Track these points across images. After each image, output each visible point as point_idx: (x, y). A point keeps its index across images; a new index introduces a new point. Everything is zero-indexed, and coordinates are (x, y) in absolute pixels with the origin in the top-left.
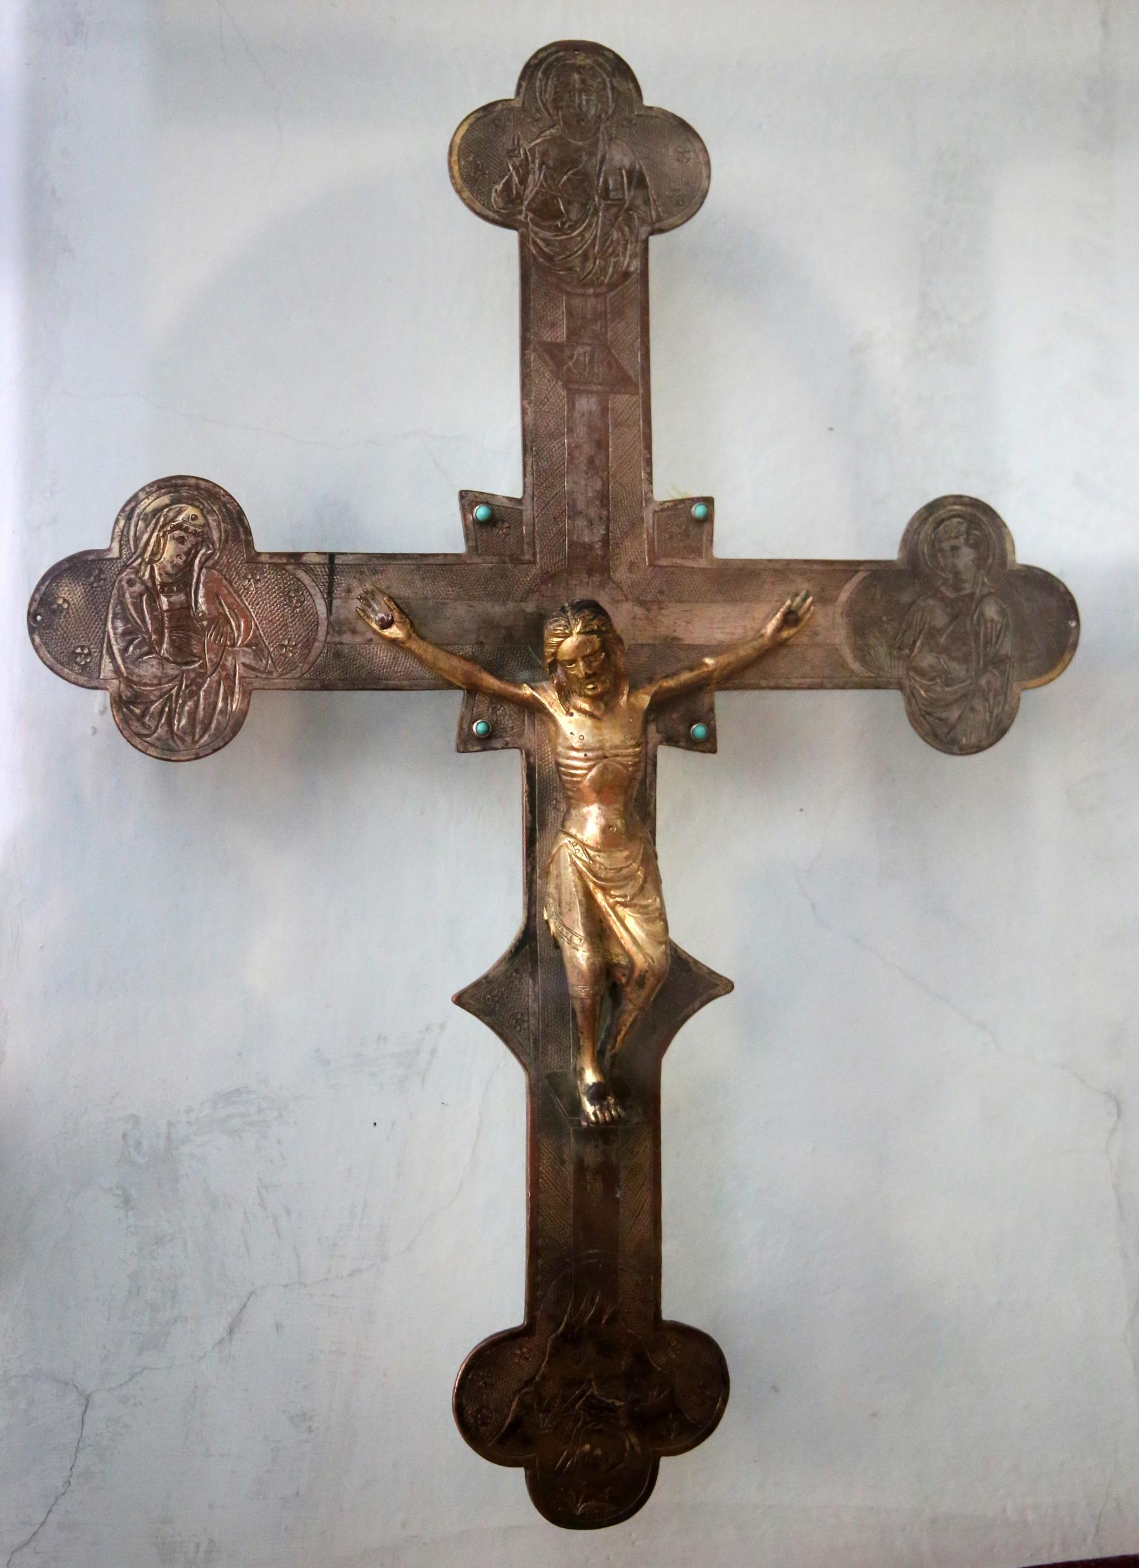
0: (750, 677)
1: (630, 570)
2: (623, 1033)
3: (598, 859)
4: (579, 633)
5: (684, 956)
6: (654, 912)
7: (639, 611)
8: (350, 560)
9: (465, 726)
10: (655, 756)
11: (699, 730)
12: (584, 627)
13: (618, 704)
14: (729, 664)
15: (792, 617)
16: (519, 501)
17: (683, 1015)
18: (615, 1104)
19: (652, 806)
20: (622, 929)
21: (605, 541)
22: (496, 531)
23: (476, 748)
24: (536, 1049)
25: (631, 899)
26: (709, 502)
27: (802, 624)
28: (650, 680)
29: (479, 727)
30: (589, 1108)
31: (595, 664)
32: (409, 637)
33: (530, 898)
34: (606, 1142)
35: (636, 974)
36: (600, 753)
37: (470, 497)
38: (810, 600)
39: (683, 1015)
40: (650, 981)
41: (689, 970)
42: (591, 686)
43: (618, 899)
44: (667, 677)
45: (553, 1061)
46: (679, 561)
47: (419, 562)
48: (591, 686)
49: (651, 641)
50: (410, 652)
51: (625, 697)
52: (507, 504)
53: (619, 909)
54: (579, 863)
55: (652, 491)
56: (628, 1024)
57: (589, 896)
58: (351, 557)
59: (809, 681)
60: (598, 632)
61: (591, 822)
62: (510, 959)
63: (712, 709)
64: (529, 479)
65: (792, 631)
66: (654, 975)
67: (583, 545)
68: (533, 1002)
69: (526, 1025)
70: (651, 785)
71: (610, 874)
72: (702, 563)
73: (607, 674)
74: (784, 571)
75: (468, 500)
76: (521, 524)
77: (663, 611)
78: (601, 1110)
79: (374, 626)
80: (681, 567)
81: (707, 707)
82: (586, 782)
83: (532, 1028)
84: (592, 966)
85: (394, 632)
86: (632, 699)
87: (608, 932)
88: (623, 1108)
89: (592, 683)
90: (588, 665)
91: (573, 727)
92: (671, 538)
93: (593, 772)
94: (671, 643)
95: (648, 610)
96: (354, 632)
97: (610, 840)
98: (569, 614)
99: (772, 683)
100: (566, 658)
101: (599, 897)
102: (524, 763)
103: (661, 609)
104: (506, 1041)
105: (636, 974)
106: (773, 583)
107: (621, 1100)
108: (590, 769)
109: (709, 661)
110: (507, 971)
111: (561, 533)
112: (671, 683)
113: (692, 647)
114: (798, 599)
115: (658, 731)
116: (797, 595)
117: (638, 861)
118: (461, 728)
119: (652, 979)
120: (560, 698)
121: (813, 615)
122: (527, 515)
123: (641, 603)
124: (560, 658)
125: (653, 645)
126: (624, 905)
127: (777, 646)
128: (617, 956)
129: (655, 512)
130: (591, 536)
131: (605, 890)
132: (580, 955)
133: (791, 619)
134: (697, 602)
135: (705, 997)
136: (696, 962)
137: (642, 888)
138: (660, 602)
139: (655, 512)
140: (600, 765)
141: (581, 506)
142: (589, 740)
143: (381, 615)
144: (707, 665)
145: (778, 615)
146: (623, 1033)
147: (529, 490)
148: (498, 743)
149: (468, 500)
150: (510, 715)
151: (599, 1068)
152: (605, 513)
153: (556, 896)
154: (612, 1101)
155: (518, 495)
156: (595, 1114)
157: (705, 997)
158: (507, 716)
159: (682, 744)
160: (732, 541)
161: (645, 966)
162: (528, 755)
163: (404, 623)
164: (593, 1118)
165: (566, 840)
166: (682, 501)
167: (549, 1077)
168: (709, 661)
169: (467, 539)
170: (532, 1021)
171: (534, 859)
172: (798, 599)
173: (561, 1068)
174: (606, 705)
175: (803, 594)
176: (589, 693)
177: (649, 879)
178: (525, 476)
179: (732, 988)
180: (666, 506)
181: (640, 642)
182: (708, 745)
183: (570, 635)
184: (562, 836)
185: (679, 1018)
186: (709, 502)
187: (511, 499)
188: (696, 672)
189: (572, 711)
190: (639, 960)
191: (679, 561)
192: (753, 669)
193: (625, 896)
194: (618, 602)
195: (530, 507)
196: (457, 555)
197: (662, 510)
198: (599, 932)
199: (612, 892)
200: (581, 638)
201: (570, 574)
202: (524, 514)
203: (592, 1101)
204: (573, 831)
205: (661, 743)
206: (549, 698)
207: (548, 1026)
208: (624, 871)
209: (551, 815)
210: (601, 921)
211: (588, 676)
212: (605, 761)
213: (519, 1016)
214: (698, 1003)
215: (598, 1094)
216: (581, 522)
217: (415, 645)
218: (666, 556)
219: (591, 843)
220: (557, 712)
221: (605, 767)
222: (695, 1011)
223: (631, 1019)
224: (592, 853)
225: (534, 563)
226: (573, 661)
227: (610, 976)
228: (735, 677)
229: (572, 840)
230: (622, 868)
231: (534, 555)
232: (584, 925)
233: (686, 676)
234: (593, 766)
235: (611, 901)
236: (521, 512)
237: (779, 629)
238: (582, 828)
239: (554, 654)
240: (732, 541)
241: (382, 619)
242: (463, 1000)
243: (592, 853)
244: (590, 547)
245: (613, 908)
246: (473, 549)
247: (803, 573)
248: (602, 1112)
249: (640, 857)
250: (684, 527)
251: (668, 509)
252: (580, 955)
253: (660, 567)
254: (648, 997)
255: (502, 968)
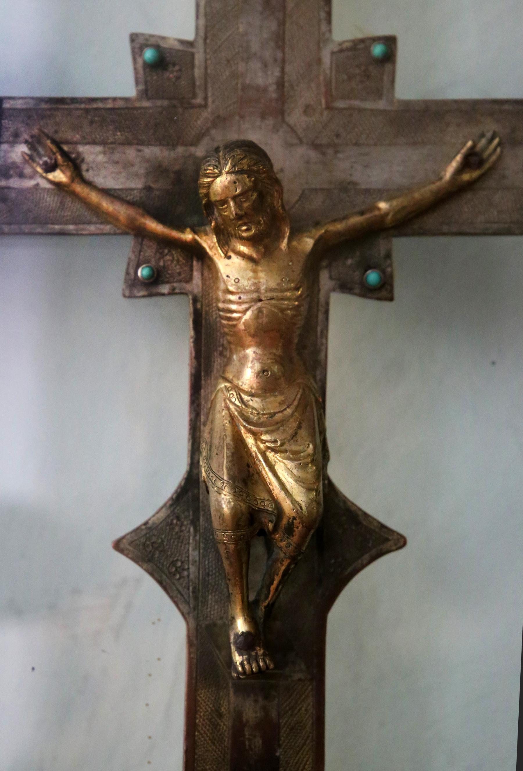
0: (431, 221)
1: (305, 112)
2: (275, 583)
3: (251, 403)
4: (227, 173)
5: (353, 509)
6: (305, 458)
7: (313, 155)
8: (19, 104)
9: (132, 271)
10: (327, 304)
11: (373, 277)
12: (234, 166)
13: (278, 248)
14: (404, 208)
15: (474, 159)
16: (191, 44)
17: (350, 569)
18: (264, 655)
19: (323, 354)
20: (270, 475)
21: (280, 84)
22: (167, 75)
23: (142, 293)
24: (196, 598)
25: (282, 445)
26: (390, 42)
27: (487, 166)
28: (317, 224)
29: (143, 272)
30: (238, 658)
31: (246, 205)
32: (73, 180)
33: (193, 445)
34: (266, 697)
35: (285, 521)
36: (255, 295)
37: (141, 40)
38: (496, 141)
39: (350, 569)
40: (298, 530)
41: (358, 523)
42: (244, 228)
43: (268, 444)
44: (335, 221)
45: (213, 609)
46: (356, 103)
47: (88, 106)
48: (244, 228)
49: (325, 186)
50: (74, 195)
51: (286, 241)
52: (178, 46)
53: (270, 455)
54: (232, 407)
55: (330, 31)
56: (280, 573)
57: (239, 442)
58: (20, 102)
59: (495, 226)
60: (249, 172)
61: (248, 369)
62: (171, 506)
63: (388, 256)
64: (202, 21)
65: (476, 174)
66: (302, 522)
67: (257, 89)
68: (194, 550)
69: (185, 573)
70: (322, 332)
71: (263, 419)
72: (381, 105)
73: (264, 216)
74: (471, 111)
75: (139, 44)
76: (193, 66)
77: (340, 155)
78: (248, 660)
79: (39, 170)
80: (360, 110)
81: (383, 252)
82: (241, 327)
83: (192, 576)
84: (234, 510)
85: (59, 176)
86: (294, 243)
87: (256, 476)
88: (272, 660)
89: (245, 224)
90: (238, 205)
91: (233, 269)
92: (350, 79)
93: (249, 314)
94: (346, 187)
95: (324, 154)
96: (21, 175)
97: (268, 385)
98: (221, 154)
99: (454, 229)
100: (218, 198)
101: (250, 441)
102: (191, 309)
103: (336, 152)
104: (165, 588)
105: (285, 521)
106: (458, 125)
107: (271, 651)
108: (245, 312)
109: (383, 205)
110: (168, 516)
111: (234, 75)
112: (339, 227)
113: (367, 191)
114: (483, 141)
115: (331, 278)
116: (482, 135)
117: (293, 407)
118: (127, 273)
119: (300, 526)
120: (219, 241)
121: (499, 158)
122: (199, 58)
123: (316, 146)
124: (213, 198)
125: (329, 190)
126: (273, 450)
127: (456, 191)
128: (263, 501)
129: (333, 53)
130: (263, 78)
131: (255, 435)
132: (224, 500)
133: (472, 160)
134: (375, 145)
135: (374, 552)
136: (366, 515)
137: (294, 436)
138: (335, 146)
139: (333, 53)
140: (255, 307)
141: (255, 47)
142: (246, 284)
143: (45, 159)
144: (379, 209)
145: (459, 158)
146: (275, 583)
147: (202, 33)
148: (165, 289)
149: (139, 44)
150: (178, 261)
151: (251, 619)
152: (279, 55)
153: (208, 440)
154: (261, 652)
155: (190, 36)
156: (242, 664)
157: (374, 552)
158: (172, 261)
159: (357, 291)
160: (411, 83)
161: (293, 513)
162: (195, 300)
163: (68, 166)
164: (240, 669)
165: (223, 385)
166: (362, 41)
167: (208, 627)
168: (383, 205)
169: (137, 82)
170: (192, 569)
171: (199, 405)
172: (483, 141)
173: (221, 618)
174: (266, 248)
175: (489, 135)
176: (244, 234)
177: (304, 425)
178: (197, 17)
179: (405, 544)
180: (345, 46)
181: (313, 186)
182: (383, 291)
183: (220, 174)
184: (221, 380)
185: (347, 572)
186: (390, 42)
187: (182, 42)
188: (367, 216)
189: (231, 254)
190: (287, 505)
191: (356, 103)
192: (426, 215)
193: (275, 441)
194: (292, 145)
195: (202, 50)
196: (126, 100)
197: (341, 51)
198: (246, 475)
199: (264, 437)
200: (232, 177)
201: (242, 117)
202: (197, 56)
203: (241, 651)
204: (230, 376)
205: (334, 290)
206: (209, 243)
207: (208, 575)
208: (278, 417)
209: (217, 362)
210: (248, 466)
211: (239, 217)
212: (259, 304)
213: (179, 564)
214: (367, 557)
215: (247, 643)
216: (255, 65)
217: (79, 188)
218: (344, 97)
219: (246, 387)
220: (216, 254)
221: (260, 310)
222: (363, 566)
223: (283, 568)
224: (246, 398)
225: (205, 106)
226: (224, 202)
227: (255, 522)
228: (413, 220)
229: (228, 385)
230: (275, 413)
231: (206, 98)
232: (228, 469)
233: (356, 220)
234: (247, 310)
235: (262, 446)
236: (193, 55)
237: (459, 171)
238: (239, 374)
239: (207, 195)
240: (411, 83)
241: (45, 163)
242: (122, 546)
243: (246, 398)
244: (265, 90)
245: (264, 454)
246: (145, 94)
247: (491, 114)
248: (249, 663)
249: (296, 403)
250: (363, 68)
251: (348, 49)
252: (224, 500)
253: (337, 109)
254: (299, 546)
255: (162, 515)
